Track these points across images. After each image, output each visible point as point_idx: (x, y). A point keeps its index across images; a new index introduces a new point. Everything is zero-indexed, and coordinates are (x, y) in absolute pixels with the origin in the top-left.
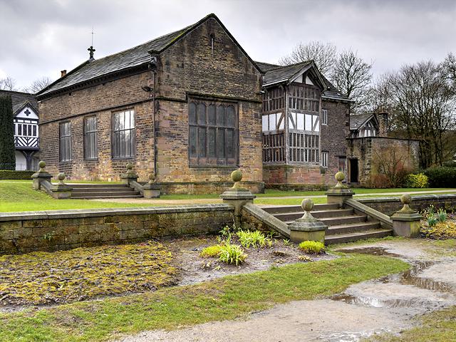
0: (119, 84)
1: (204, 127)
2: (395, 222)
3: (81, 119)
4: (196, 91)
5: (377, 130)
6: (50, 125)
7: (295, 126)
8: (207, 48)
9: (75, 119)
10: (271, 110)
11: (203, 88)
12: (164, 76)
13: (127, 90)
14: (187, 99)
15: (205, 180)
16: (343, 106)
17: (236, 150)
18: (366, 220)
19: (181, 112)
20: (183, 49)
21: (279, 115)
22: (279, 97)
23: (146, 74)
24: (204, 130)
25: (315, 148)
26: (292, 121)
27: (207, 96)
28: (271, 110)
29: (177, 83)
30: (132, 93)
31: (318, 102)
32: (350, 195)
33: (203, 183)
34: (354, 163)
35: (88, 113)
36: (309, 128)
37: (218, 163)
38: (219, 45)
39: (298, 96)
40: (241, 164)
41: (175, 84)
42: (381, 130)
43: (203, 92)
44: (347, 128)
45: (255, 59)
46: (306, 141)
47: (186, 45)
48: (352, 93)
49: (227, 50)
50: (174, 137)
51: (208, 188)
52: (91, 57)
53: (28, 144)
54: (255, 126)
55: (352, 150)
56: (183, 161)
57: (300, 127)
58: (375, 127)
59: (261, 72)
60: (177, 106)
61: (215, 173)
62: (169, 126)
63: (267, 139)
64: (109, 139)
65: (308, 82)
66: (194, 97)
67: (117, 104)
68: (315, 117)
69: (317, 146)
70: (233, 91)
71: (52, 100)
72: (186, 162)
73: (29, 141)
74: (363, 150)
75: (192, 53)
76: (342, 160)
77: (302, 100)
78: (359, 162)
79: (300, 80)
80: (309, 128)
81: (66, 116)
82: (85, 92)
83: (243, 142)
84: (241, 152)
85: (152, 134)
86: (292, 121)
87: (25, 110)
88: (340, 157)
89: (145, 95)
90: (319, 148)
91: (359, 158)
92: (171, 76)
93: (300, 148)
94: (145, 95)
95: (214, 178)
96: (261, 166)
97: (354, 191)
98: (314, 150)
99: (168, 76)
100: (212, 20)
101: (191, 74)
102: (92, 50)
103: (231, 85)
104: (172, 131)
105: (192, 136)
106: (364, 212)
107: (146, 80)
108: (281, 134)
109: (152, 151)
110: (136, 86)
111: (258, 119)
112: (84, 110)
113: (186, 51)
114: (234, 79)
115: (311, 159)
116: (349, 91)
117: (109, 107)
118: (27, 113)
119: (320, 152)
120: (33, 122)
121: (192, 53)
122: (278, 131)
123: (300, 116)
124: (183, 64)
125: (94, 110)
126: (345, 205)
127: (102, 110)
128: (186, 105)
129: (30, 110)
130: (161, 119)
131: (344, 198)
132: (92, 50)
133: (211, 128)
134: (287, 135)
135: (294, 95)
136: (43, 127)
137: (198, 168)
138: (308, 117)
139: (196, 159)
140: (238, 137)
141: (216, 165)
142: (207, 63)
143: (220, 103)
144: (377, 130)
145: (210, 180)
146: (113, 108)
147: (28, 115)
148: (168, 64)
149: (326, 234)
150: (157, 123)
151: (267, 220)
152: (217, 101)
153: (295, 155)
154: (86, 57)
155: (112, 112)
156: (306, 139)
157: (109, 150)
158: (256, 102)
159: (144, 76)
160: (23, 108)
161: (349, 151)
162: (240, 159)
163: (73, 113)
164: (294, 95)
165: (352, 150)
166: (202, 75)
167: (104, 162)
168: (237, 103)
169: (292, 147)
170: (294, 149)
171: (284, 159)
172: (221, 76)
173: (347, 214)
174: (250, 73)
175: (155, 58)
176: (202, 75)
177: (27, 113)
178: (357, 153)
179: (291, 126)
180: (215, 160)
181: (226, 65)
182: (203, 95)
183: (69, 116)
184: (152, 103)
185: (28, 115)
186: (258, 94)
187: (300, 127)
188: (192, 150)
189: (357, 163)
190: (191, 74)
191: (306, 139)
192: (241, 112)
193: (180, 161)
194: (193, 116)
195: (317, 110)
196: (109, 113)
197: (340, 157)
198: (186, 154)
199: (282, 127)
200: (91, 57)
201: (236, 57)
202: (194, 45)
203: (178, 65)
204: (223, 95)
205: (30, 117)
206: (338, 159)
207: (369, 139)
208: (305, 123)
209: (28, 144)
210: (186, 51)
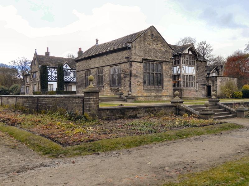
0: (114, 55)
1: (149, 73)
2: (238, 112)
3: (96, 69)
4: (146, 58)
5: (218, 73)
6: (81, 72)
7: (185, 72)
8: (150, 40)
9: (93, 69)
10: (174, 65)
11: (149, 56)
12: (133, 52)
13: (117, 57)
14: (142, 61)
15: (149, 95)
16: (204, 63)
17: (162, 82)
18: (225, 111)
19: (140, 67)
20: (141, 41)
21: (178, 67)
22: (178, 59)
23: (126, 51)
24: (149, 74)
25: (193, 81)
26: (184, 69)
27: (151, 60)
28: (174, 65)
29: (139, 55)
30: (119, 59)
31: (194, 61)
32: (218, 101)
33: (149, 96)
34: (209, 87)
35: (99, 67)
36: (191, 73)
37: (155, 88)
38: (155, 38)
39: (186, 59)
40: (164, 88)
41: (138, 55)
42: (220, 73)
43: (149, 58)
44: (206, 72)
45: (169, 43)
46: (189, 78)
47: (142, 39)
48: (205, 56)
49: (158, 41)
50: (138, 77)
51: (151, 98)
52: (97, 43)
53: (66, 80)
54: (170, 72)
55: (208, 82)
56: (141, 87)
57: (187, 72)
58: (217, 72)
59: (172, 49)
60: (139, 64)
61: (154, 92)
62: (135, 72)
63: (176, 77)
64: (109, 78)
65: (190, 53)
66: (145, 61)
67: (112, 64)
68: (193, 68)
69: (194, 80)
70: (161, 57)
71: (82, 61)
72: (142, 87)
73: (55, 78)
74: (213, 82)
75: (144, 42)
76: (203, 86)
77: (188, 61)
78: (211, 87)
79: (187, 52)
80: (191, 73)
81: (89, 68)
82: (98, 58)
83: (165, 79)
84: (164, 83)
85: (128, 76)
86: (184, 69)
87: (65, 65)
88: (203, 85)
89: (126, 60)
90: (195, 81)
91: (211, 85)
92: (136, 52)
93: (187, 81)
94: (126, 60)
95: (153, 94)
96: (172, 89)
97: (220, 99)
98: (193, 82)
99: (135, 52)
100: (152, 28)
101: (144, 51)
102: (97, 40)
103: (160, 55)
104: (137, 75)
105: (144, 76)
106: (224, 107)
107: (125, 54)
108: (179, 75)
109: (128, 83)
110: (121, 56)
111: (171, 69)
112: (97, 65)
113: (142, 42)
114: (161, 53)
115: (192, 86)
116: (204, 55)
117: (109, 64)
118: (66, 66)
119: (195, 82)
120: (68, 70)
121: (144, 42)
122: (178, 74)
123: (187, 67)
124: (141, 47)
125: (102, 66)
126: (216, 105)
127: (106, 66)
128: (142, 64)
129: (67, 65)
130: (132, 70)
131: (216, 102)
132: (97, 40)
133: (152, 73)
134: (182, 76)
135: (184, 59)
136: (78, 73)
137: (147, 90)
138: (190, 68)
139: (146, 86)
140: (163, 77)
141: (154, 88)
142: (150, 46)
143: (156, 63)
144: (218, 73)
145: (152, 95)
146: (111, 65)
147: (66, 67)
148: (135, 47)
149: (214, 116)
150: (131, 71)
151: (190, 110)
152: (154, 62)
153: (186, 84)
154: (95, 43)
155: (110, 67)
156: (189, 77)
157: (109, 83)
158: (170, 62)
159: (125, 52)
160: (65, 64)
161: (207, 82)
162: (164, 86)
163: (92, 67)
164: (184, 59)
165: (208, 82)
166: (149, 51)
167: (106, 87)
168: (162, 62)
169: (190, 81)
170: (185, 82)
171: (180, 86)
172: (156, 51)
173: (217, 108)
174: (168, 50)
175: (130, 45)
176: (149, 51)
177: (66, 66)
178: (210, 83)
179: (183, 72)
180: (154, 86)
181: (158, 47)
182: (149, 60)
183: (90, 68)
184: (128, 63)
185: (66, 67)
186: (171, 59)
187: (187, 72)
188: (145, 83)
189: (211, 88)
190: (144, 51)
191: (189, 77)
192: (164, 66)
193: (140, 87)
194: (145, 68)
195: (194, 65)
196: (109, 67)
197: (203, 85)
198: (142, 84)
199: (179, 72)
200: (97, 43)
201: (162, 43)
202: (145, 39)
203: (139, 47)
204: (157, 59)
205: (67, 68)
206: (202, 86)
207: (216, 77)
208: (189, 70)
209: (66, 80)
210: (142, 42)
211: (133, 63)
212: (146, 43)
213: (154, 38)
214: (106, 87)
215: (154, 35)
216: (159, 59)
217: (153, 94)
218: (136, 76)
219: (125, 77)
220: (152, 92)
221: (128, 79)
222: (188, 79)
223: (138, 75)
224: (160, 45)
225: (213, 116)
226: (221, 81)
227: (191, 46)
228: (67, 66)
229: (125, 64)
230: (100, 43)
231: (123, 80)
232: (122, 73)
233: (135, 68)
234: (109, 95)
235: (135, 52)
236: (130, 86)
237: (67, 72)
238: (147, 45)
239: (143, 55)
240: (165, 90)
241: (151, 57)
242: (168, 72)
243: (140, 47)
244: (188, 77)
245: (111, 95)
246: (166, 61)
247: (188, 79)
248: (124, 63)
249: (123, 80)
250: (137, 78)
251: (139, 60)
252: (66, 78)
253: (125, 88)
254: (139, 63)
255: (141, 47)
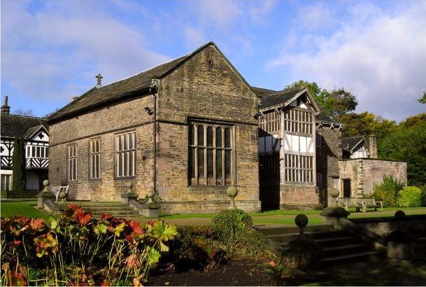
3: (87, 139)
20: (183, 75)
26: (288, 143)
47: (185, 71)
49: (225, 76)
50: (173, 158)
53: (41, 165)
61: (213, 193)
62: (168, 147)
64: (112, 160)
67: (120, 126)
70: (231, 113)
80: (303, 150)
82: (91, 115)
85: (152, 155)
86: (288, 143)
89: (147, 118)
102: (99, 78)
103: (229, 108)
109: (152, 172)
117: (113, 129)
120: (46, 144)
123: (295, 138)
124: (182, 89)
132: (99, 78)
138: (303, 139)
142: (206, 88)
157: (112, 171)
163: (79, 136)
172: (219, 100)
181: (225, 89)
190: (191, 98)
193: (179, 180)
204: (221, 118)
205: (43, 139)
209: (41, 165)
211: (162, 125)
212: (196, 81)
213: (213, 70)
214: (107, 182)
215: (215, 62)
216: (227, 118)
217: (211, 197)
218: (169, 156)
219: (144, 158)
220: (209, 193)
221: (151, 162)
222: (297, 163)
223: (176, 153)
224: (229, 86)
225: (413, 243)
226: (373, 169)
227: (304, 91)
228: (43, 136)
229: (145, 127)
230: (105, 83)
231: (141, 165)
232: (139, 149)
233: (167, 137)
234: (112, 199)
235: (168, 100)
236: (155, 180)
237: (43, 149)
238: (197, 84)
239: (186, 107)
240: (241, 189)
241: (208, 112)
242: (247, 148)
243: (180, 88)
244: (297, 159)
245: (117, 200)
246: (244, 121)
247: (297, 163)
248: (142, 125)
249: (141, 165)
250: (171, 160)
251: (176, 119)
252: (41, 161)
253: (144, 183)
254: (178, 126)
255: (182, 89)
